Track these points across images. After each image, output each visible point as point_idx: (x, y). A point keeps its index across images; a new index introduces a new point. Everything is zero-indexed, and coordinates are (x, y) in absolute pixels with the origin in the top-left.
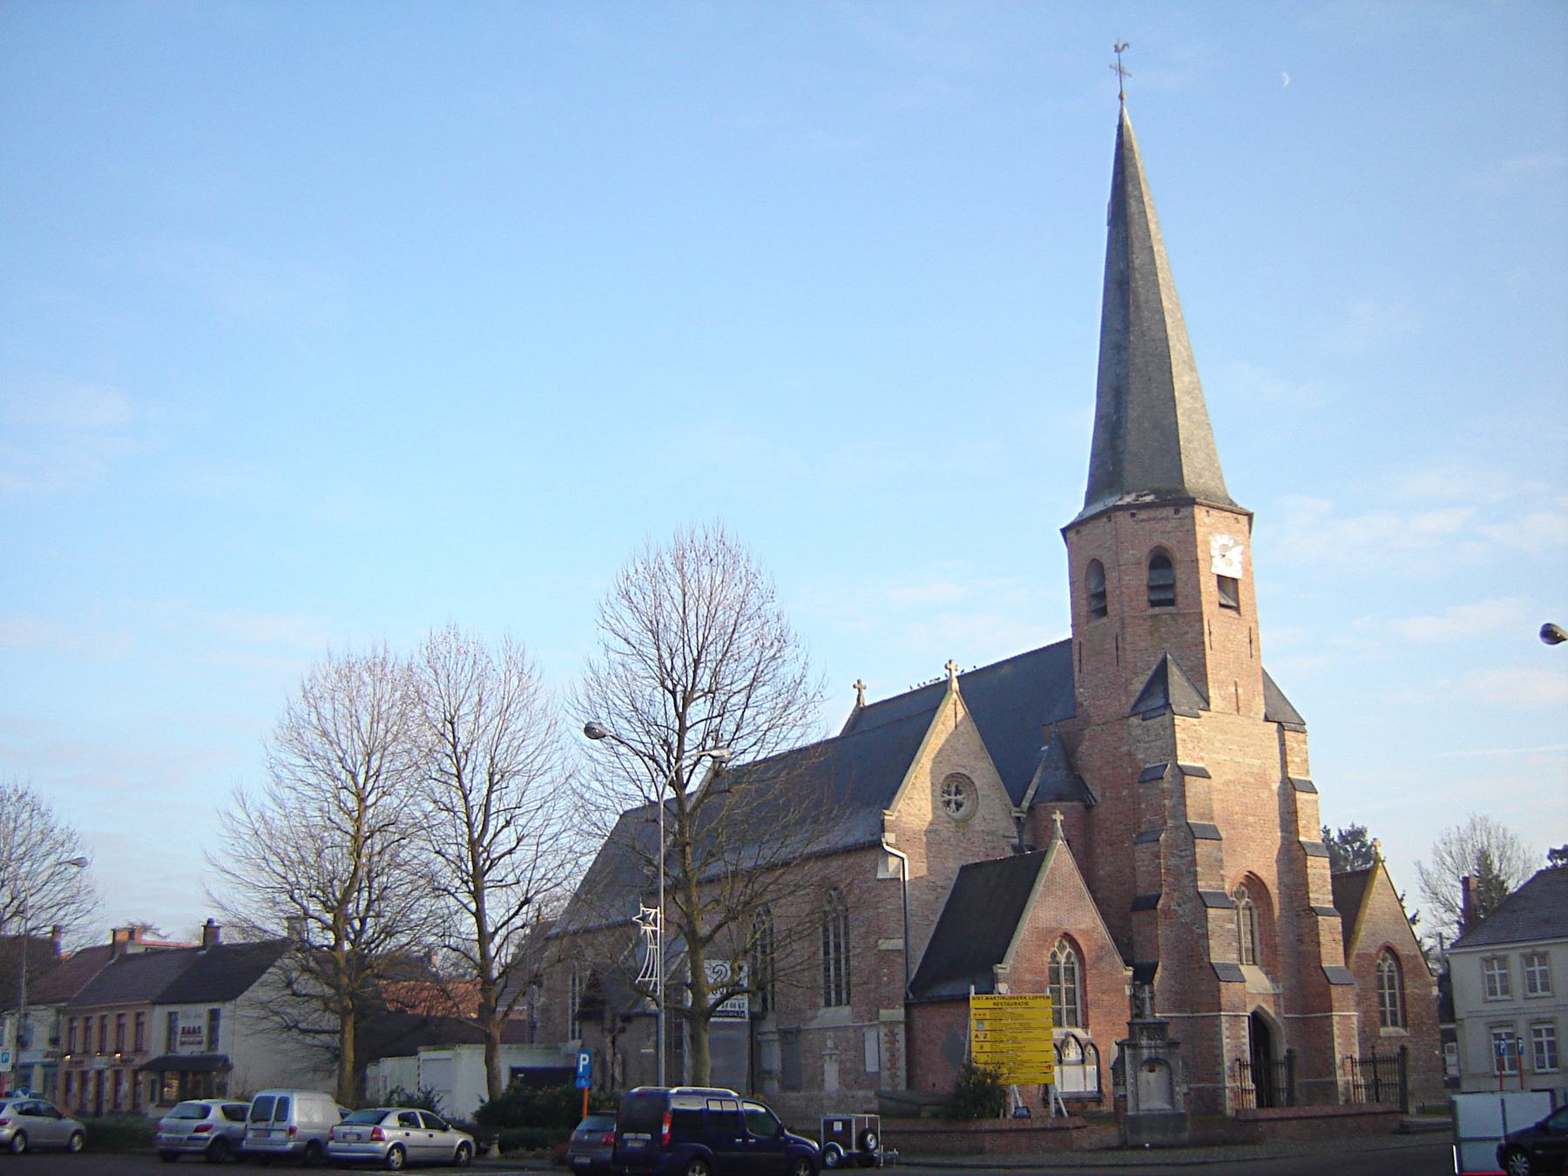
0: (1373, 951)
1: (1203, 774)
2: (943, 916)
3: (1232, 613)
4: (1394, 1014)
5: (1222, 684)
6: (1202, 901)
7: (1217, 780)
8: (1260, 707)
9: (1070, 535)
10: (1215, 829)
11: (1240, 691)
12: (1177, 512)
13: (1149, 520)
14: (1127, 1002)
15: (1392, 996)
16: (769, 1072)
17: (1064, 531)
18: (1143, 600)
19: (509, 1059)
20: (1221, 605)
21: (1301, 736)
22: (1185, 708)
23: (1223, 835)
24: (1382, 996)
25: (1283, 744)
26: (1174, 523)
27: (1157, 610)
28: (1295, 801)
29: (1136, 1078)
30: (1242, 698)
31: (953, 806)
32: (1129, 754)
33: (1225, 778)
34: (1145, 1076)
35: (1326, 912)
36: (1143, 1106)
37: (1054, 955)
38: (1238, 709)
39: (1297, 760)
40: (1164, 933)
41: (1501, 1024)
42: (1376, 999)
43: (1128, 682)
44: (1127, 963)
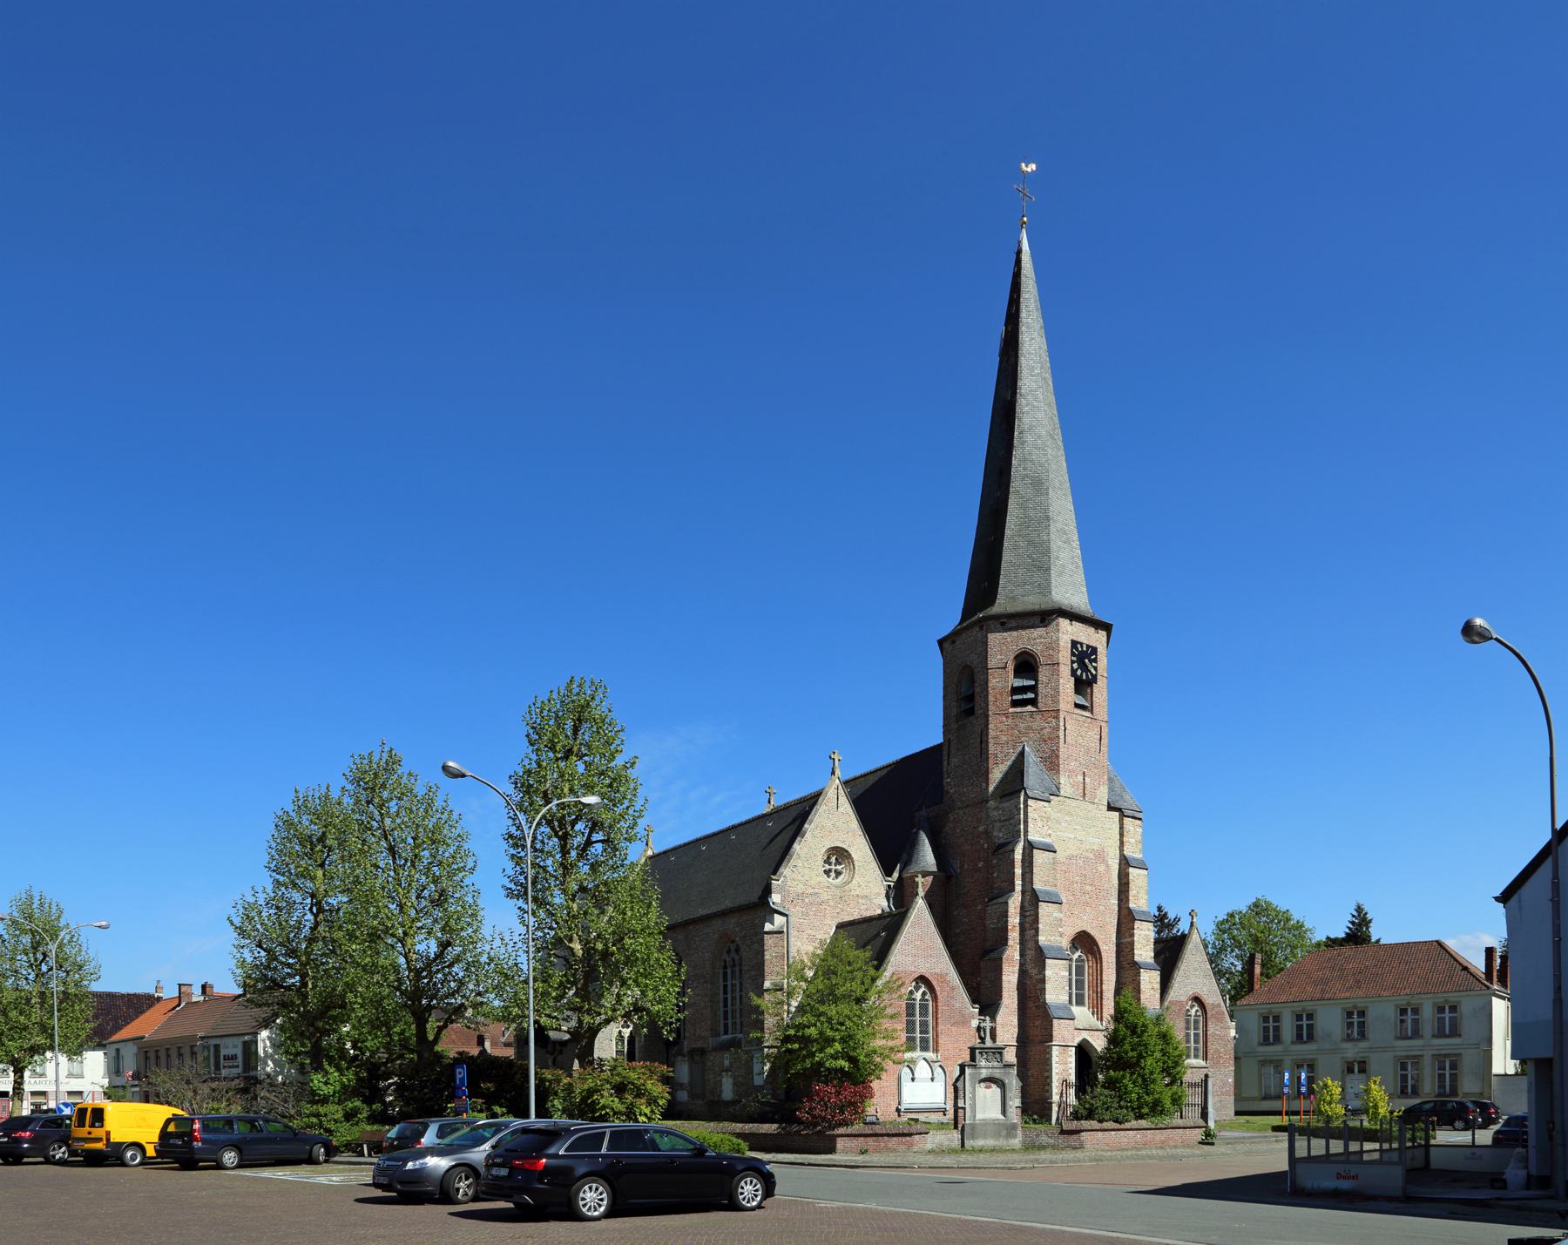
0: (1183, 999)
1: (1049, 849)
3: (1087, 714)
4: (1196, 1049)
7: (1061, 855)
9: (946, 645)
17: (941, 642)
20: (1077, 706)
22: (1036, 793)
24: (1188, 1035)
25: (1121, 828)
29: (974, 1093)
33: (1069, 852)
34: (981, 1090)
35: (1148, 968)
36: (979, 1116)
40: (1010, 978)
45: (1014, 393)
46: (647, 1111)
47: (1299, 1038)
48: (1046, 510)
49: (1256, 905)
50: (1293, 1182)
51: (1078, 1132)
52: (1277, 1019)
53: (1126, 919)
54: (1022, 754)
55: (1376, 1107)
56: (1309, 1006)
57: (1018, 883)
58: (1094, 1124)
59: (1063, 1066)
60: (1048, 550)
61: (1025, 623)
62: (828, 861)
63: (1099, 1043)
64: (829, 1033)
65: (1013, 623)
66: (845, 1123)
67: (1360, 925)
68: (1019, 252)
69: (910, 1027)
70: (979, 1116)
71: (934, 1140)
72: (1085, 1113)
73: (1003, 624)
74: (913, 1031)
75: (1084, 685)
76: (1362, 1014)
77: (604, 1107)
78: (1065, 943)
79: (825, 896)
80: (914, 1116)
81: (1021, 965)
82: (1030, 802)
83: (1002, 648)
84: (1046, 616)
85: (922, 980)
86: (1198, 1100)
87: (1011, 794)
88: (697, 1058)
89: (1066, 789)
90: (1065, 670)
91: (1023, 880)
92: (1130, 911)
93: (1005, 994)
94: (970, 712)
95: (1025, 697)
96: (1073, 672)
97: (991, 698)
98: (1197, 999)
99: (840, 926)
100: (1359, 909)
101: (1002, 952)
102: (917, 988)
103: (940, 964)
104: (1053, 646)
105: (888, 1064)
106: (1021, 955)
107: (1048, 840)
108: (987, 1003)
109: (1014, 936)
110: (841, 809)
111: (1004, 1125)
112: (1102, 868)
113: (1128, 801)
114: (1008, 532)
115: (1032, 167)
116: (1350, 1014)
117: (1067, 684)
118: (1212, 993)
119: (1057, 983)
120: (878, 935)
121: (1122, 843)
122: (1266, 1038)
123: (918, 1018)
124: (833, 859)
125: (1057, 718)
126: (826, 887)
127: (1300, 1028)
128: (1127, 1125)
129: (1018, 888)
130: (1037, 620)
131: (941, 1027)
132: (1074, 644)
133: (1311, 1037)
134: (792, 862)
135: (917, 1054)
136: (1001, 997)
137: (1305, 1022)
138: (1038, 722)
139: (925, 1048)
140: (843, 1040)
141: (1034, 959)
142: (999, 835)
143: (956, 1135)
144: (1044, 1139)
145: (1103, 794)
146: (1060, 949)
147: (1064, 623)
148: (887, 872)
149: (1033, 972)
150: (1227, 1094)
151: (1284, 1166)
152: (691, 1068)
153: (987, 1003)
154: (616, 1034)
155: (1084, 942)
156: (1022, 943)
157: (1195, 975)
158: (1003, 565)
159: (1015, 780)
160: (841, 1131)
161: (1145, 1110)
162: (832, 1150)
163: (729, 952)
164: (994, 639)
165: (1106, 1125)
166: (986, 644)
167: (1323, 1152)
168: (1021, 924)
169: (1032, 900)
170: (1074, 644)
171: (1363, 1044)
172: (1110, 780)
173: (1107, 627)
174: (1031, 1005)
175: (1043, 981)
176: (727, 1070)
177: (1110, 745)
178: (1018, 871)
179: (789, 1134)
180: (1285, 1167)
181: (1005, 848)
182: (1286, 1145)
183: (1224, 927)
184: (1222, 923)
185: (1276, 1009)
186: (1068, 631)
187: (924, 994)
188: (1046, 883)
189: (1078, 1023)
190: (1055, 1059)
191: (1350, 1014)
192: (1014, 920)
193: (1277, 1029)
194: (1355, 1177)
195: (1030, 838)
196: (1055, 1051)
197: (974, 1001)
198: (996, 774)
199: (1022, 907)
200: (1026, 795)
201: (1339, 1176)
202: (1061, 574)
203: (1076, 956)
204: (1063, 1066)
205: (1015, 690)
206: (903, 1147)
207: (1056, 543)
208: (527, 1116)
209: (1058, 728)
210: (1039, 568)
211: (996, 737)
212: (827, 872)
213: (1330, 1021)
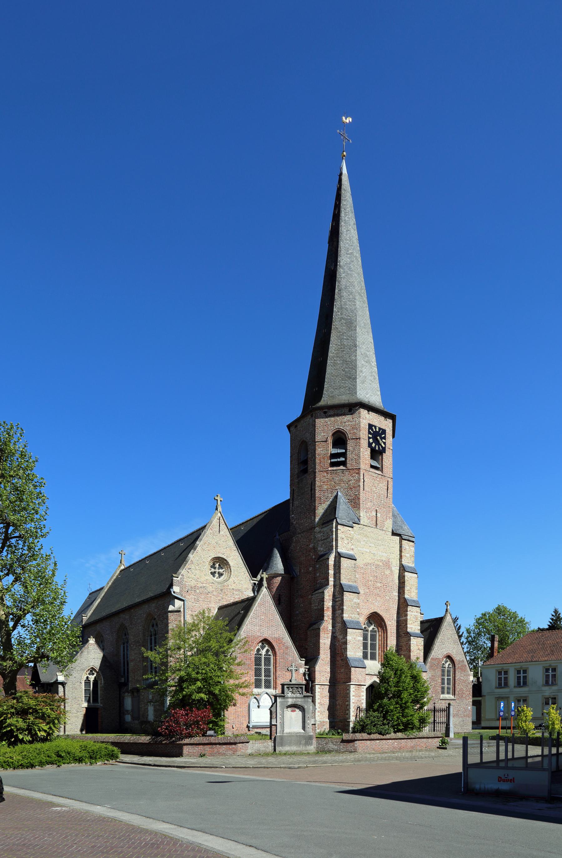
0: (440, 657)
1: (352, 558)
4: (448, 688)
5: (368, 510)
9: (292, 429)
11: (379, 515)
16: (127, 711)
17: (289, 427)
20: (372, 467)
23: (362, 592)
24: (443, 680)
25: (401, 547)
27: (335, 468)
28: (404, 576)
30: (379, 519)
31: (217, 575)
32: (314, 548)
34: (288, 713)
35: (416, 636)
36: (287, 730)
40: (325, 641)
42: (440, 681)
45: (336, 265)
46: (46, 728)
47: (519, 685)
48: (355, 340)
49: (498, 609)
50: (466, 783)
51: (353, 741)
52: (506, 673)
53: (403, 605)
54: (336, 497)
55: (553, 724)
56: (524, 665)
57: (331, 579)
58: (365, 736)
59: (358, 698)
60: (355, 366)
61: (339, 412)
62: (213, 566)
64: (194, 675)
65: (331, 412)
66: (190, 736)
67: (556, 620)
68: (341, 174)
69: (258, 673)
70: (287, 730)
71: (253, 747)
72: (359, 728)
73: (325, 413)
74: (260, 675)
75: (377, 453)
76: (554, 670)
77: (10, 725)
78: (362, 619)
79: (210, 589)
80: (259, 730)
81: (333, 633)
82: (339, 527)
83: (325, 428)
84: (352, 407)
85: (265, 641)
86: (444, 719)
87: (328, 522)
88: (135, 694)
89: (364, 520)
90: (364, 443)
91: (335, 578)
92: (405, 600)
93: (322, 651)
94: (305, 471)
95: (339, 460)
96: (370, 445)
97: (317, 461)
98: (449, 657)
99: (220, 608)
100: (556, 611)
101: (320, 625)
102: (263, 648)
103: (278, 631)
104: (357, 427)
105: (236, 696)
106: (333, 627)
107: (351, 552)
108: (309, 655)
109: (328, 614)
110: (222, 533)
111: (303, 736)
112: (387, 572)
113: (406, 530)
114: (330, 354)
115: (349, 120)
116: (547, 670)
117: (365, 453)
118: (459, 655)
119: (354, 647)
120: (239, 613)
121: (401, 557)
122: (500, 684)
123: (263, 667)
124: (217, 565)
125: (359, 473)
126: (211, 582)
127: (519, 678)
128: (388, 736)
129: (331, 583)
130: (346, 410)
131: (278, 673)
132: (370, 426)
133: (525, 684)
134: (187, 566)
135: (263, 690)
136: (319, 654)
137: (522, 675)
138: (347, 477)
139: (268, 686)
140: (204, 680)
141: (341, 628)
142: (321, 549)
143: (270, 744)
144: (331, 746)
145: (389, 525)
146: (358, 623)
147: (363, 412)
148: (254, 574)
149: (340, 637)
150: (467, 716)
151: (459, 769)
152: (132, 701)
153: (309, 655)
154: (85, 678)
155: (375, 619)
156: (334, 618)
157: (447, 643)
158: (327, 376)
159: (331, 513)
160: (187, 741)
161: (401, 727)
162: (180, 754)
163: (153, 626)
164: (320, 423)
165: (372, 736)
166: (314, 426)
167: (478, 761)
168: (333, 607)
169: (340, 590)
170: (370, 426)
171: (554, 688)
172: (394, 516)
173: (392, 417)
174: (338, 659)
175: (346, 643)
176: (151, 702)
177: (394, 494)
178: (331, 572)
179: (156, 743)
180: (460, 769)
181: (323, 558)
182: (495, 749)
183: (482, 621)
184: (479, 619)
185: (506, 667)
186: (366, 418)
188: (349, 580)
189: (368, 671)
190: (352, 693)
191: (547, 670)
192: (328, 604)
193: (506, 679)
194: (512, 780)
195: (339, 550)
196: (352, 688)
197: (301, 656)
198: (320, 511)
199: (334, 596)
200: (337, 524)
201: (500, 779)
202: (363, 382)
203: (370, 629)
204: (358, 698)
205: (333, 456)
206: (231, 752)
207: (360, 362)
210: (350, 378)
211: (321, 486)
212: (213, 574)
213: (536, 674)
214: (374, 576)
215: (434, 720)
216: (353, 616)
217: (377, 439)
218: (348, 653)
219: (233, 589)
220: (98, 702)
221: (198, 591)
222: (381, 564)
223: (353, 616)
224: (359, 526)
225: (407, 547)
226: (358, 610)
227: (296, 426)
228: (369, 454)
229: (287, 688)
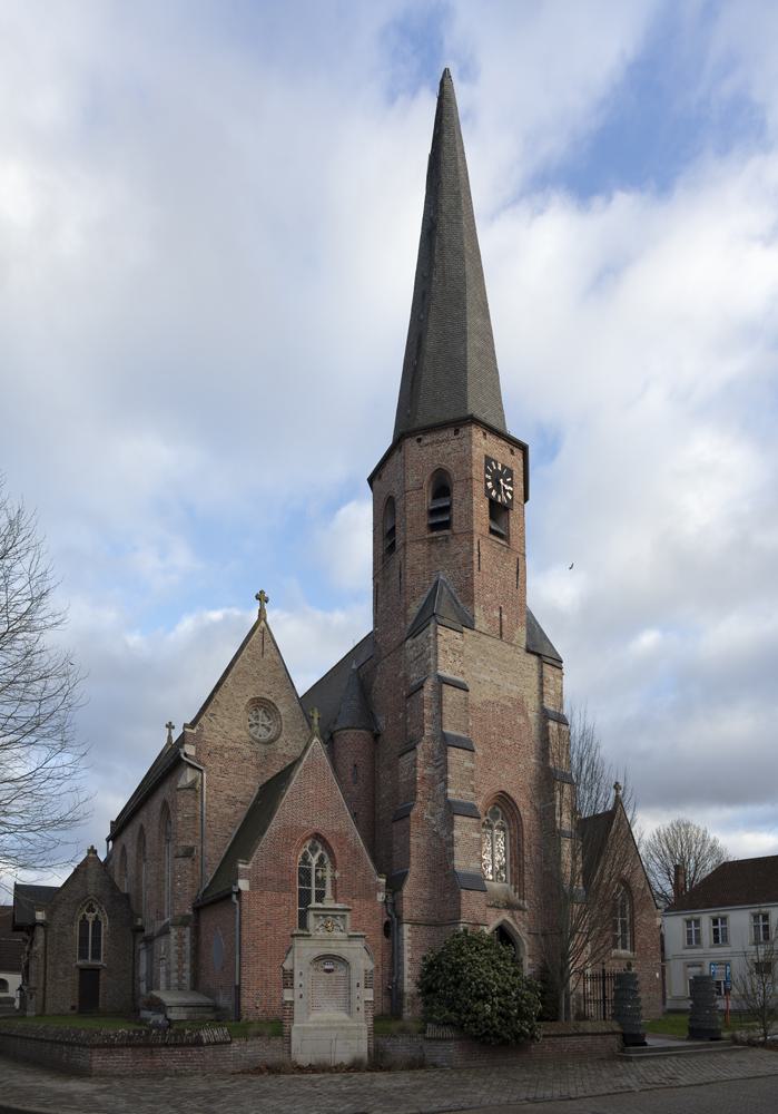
2: (238, 831)
6: (452, 810)
8: (521, 635)
9: (375, 483)
10: (469, 741)
11: (504, 617)
12: (456, 432)
13: (431, 444)
14: (378, 908)
15: (623, 923)
18: (423, 528)
19: (407, 998)
21: (558, 672)
23: (479, 751)
25: (541, 677)
26: (454, 444)
27: (435, 534)
30: (505, 624)
33: (484, 697)
37: (305, 859)
38: (501, 635)
39: (552, 692)
40: (417, 842)
41: (694, 965)
43: (407, 606)
44: (380, 872)
63: (102, 857)
89: (481, 624)
96: (488, 491)
102: (313, 849)
104: (466, 461)
107: (460, 678)
112: (521, 720)
117: (481, 507)
121: (542, 694)
122: (690, 941)
125: (471, 541)
132: (488, 460)
133: (725, 939)
147: (477, 434)
154: (80, 917)
170: (488, 460)
187: (321, 859)
193: (698, 932)
205: (433, 513)
208: (87, 958)
209: (471, 553)
214: (499, 726)
215: (604, 981)
216: (463, 793)
217: (499, 483)
218: (456, 862)
219: (285, 755)
220: (99, 958)
221: (226, 755)
222: (510, 705)
223: (463, 793)
224: (473, 633)
225: (552, 678)
226: (472, 783)
227: (380, 477)
228: (487, 507)
229: (316, 916)
